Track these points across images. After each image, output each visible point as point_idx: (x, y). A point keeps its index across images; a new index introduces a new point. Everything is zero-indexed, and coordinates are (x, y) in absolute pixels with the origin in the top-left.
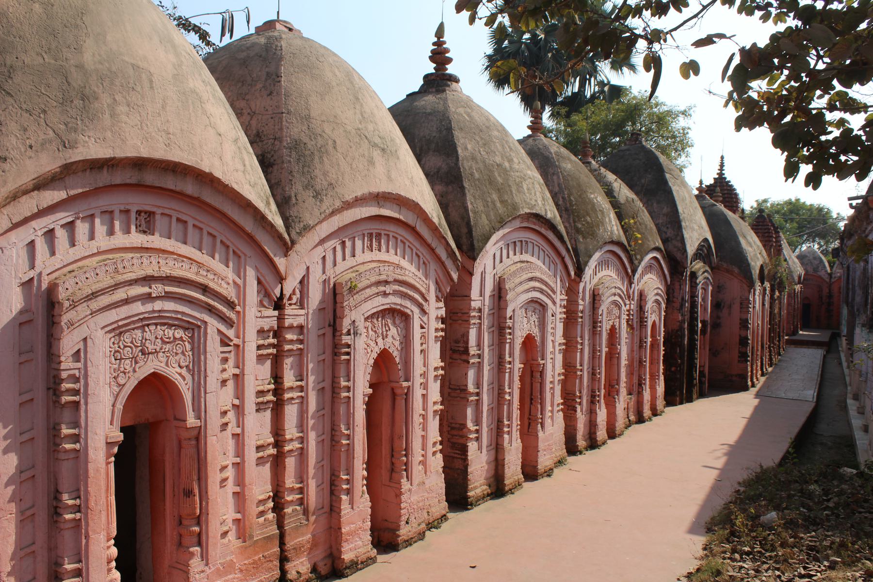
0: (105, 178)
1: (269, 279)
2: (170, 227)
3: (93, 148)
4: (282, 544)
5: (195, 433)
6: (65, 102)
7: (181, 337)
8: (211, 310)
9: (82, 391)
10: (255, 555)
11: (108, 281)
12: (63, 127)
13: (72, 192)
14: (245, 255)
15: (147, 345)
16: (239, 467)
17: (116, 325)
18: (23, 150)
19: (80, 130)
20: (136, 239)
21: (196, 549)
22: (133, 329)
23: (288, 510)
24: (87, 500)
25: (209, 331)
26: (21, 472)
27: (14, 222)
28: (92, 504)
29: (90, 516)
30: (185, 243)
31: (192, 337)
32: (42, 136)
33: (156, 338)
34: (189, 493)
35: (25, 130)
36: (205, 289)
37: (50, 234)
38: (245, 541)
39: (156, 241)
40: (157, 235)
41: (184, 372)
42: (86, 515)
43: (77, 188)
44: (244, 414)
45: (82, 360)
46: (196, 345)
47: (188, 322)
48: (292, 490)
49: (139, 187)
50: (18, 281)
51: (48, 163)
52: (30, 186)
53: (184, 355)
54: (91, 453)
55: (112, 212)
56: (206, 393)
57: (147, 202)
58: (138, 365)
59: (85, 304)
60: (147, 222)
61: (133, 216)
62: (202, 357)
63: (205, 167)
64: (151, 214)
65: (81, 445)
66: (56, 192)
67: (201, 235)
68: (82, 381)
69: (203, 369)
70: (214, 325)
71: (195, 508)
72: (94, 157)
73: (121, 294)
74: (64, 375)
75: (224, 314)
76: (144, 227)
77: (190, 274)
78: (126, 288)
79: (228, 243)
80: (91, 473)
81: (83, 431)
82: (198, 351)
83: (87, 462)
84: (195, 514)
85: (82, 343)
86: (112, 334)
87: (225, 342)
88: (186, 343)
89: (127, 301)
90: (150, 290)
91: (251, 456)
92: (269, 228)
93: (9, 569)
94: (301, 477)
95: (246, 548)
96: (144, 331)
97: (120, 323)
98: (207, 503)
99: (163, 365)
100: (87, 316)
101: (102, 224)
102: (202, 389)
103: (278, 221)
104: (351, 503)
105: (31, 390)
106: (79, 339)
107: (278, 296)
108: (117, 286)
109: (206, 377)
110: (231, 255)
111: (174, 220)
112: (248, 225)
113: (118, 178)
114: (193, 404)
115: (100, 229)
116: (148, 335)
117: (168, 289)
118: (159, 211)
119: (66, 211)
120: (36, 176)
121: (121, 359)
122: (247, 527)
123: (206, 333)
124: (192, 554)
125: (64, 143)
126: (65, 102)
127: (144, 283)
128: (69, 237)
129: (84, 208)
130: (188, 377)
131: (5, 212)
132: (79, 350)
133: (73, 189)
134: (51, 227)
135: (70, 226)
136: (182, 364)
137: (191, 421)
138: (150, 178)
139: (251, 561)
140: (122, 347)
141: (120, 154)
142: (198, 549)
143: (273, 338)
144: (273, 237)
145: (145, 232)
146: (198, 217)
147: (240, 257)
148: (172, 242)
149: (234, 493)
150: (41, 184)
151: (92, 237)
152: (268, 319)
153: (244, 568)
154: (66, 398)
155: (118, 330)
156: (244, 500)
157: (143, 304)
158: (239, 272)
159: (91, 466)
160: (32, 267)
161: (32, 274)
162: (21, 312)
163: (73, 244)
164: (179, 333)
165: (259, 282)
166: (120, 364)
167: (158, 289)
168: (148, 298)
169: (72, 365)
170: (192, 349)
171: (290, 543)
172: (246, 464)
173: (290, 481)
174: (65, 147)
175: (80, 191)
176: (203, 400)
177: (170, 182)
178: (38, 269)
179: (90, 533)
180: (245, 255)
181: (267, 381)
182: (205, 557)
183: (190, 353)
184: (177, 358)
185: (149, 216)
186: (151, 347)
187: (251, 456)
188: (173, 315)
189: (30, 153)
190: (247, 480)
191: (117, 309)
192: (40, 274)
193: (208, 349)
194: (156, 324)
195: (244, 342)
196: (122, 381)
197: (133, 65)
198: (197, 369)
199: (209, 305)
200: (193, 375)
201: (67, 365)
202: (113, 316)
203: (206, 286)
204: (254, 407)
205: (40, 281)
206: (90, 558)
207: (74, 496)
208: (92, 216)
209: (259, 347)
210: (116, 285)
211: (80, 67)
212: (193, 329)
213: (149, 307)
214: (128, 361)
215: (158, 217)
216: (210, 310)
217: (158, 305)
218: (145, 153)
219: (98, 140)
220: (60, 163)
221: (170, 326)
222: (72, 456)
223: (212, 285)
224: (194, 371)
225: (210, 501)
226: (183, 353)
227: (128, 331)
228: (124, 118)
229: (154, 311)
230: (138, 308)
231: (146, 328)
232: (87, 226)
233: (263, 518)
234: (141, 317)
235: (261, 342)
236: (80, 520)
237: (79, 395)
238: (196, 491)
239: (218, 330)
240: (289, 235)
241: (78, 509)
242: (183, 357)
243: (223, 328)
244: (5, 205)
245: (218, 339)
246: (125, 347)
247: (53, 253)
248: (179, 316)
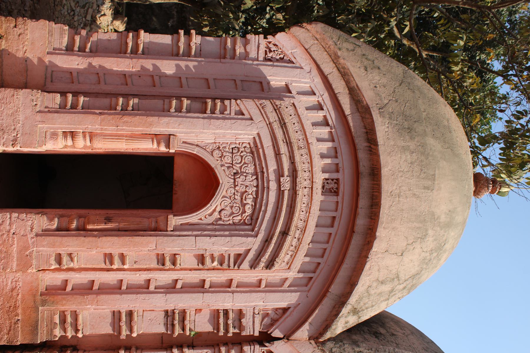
0: (361, 144)
1: (288, 321)
2: (328, 211)
3: (382, 129)
5: (162, 226)
7: (245, 212)
8: (267, 241)
9: (213, 115)
10: (23, 309)
12: (390, 110)
13: (350, 118)
14: (308, 291)
15: (242, 177)
17: (259, 146)
18: (373, 82)
19: (391, 121)
20: (320, 177)
21: (55, 224)
22: (255, 165)
24: (130, 115)
25: (250, 239)
26: (160, 77)
27: (328, 76)
28: (126, 119)
29: (117, 116)
30: (316, 226)
31: (245, 224)
32: (383, 96)
33: (247, 186)
35: (384, 87)
36: (285, 233)
37: (320, 107)
38: (41, 295)
39: (318, 197)
40: (322, 198)
41: (216, 215)
42: (118, 114)
43: (353, 122)
44: (166, 293)
45: (236, 116)
46: (238, 227)
47: (257, 219)
49: (357, 174)
50: (289, 82)
51: (369, 96)
52: (353, 84)
53: (230, 215)
54: (165, 120)
55: (336, 157)
56: (196, 236)
57: (346, 187)
58: (226, 169)
59: (277, 118)
60: (331, 189)
61: (335, 176)
62: (227, 233)
63: (381, 232)
64: (336, 193)
65: (173, 112)
66: (349, 106)
67: (323, 243)
68: (221, 116)
69: (217, 233)
70: (254, 244)
71: (94, 223)
72: (377, 129)
73: (283, 149)
74: (227, 102)
75: (263, 255)
76: (327, 186)
77: (297, 221)
78: (288, 154)
79: (318, 271)
80: (151, 119)
81: (183, 114)
82: (233, 229)
83: (159, 116)
84: (89, 223)
85: (249, 117)
86: (252, 145)
87: (239, 258)
88: (239, 218)
89: (278, 154)
90: (286, 176)
91: (124, 303)
92: (334, 313)
93: (94, 64)
95: (34, 296)
96: (253, 175)
97: (261, 150)
98: (95, 236)
99: (224, 193)
100: (268, 119)
101: (328, 148)
102: (199, 233)
103: (339, 327)
105: (216, 88)
106: (252, 114)
107: (273, 335)
109: (210, 236)
110: (309, 273)
111: (329, 230)
112: (335, 289)
113: (362, 155)
114: (187, 224)
116: (249, 177)
117: (286, 193)
119: (336, 119)
120: (360, 86)
121: (232, 153)
122: (56, 298)
123: (247, 236)
124: (51, 220)
125: (382, 109)
127: (291, 171)
128: (318, 122)
129: (339, 132)
130: (211, 220)
131: (334, 70)
132: (243, 114)
133: (352, 119)
134: (325, 108)
135: (326, 123)
136: (223, 212)
137: (174, 221)
138: (365, 183)
139: (19, 303)
140: (242, 154)
141: (382, 149)
142: (55, 226)
143: (233, 333)
144: (327, 320)
145: (323, 187)
146: (337, 237)
147: (307, 286)
148: (318, 213)
149: (93, 281)
150: (354, 93)
151: (319, 140)
152: (251, 323)
153: (15, 294)
156: (83, 294)
157: (274, 170)
158: (295, 285)
159: (155, 119)
160: (299, 93)
161: (294, 92)
163: (314, 124)
164: (249, 210)
165: (285, 310)
166: (228, 152)
168: (280, 174)
169: (234, 108)
170: (234, 224)
172: (118, 296)
174: (379, 109)
175: (351, 124)
176: (190, 233)
177: (363, 202)
178: (297, 96)
179: (102, 116)
180: (308, 291)
181: (192, 328)
182: (46, 233)
183: (231, 222)
184: (228, 208)
185: (335, 192)
187: (124, 303)
188: (264, 202)
189: (372, 86)
191: (272, 147)
192: (294, 98)
193: (234, 238)
194: (257, 186)
195: (233, 292)
196: (217, 153)
197: (434, 175)
198: (217, 228)
199: (271, 238)
200: (212, 224)
201: (233, 106)
202: (267, 143)
203: (287, 234)
204: (170, 307)
205: (289, 97)
206: (83, 115)
207: (134, 107)
208: (333, 141)
209: (226, 312)
210: (291, 143)
212: (251, 224)
213: (272, 177)
214: (230, 159)
215: (334, 199)
216: (267, 241)
217: (273, 185)
218: (385, 171)
219: (387, 133)
220: (369, 103)
221: (255, 200)
222: (166, 107)
223: (289, 238)
224: (216, 225)
225: (97, 239)
226: (233, 213)
227: (253, 158)
228: (404, 157)
229: (268, 181)
230: (272, 166)
231: (254, 177)
232: (326, 136)
233: (57, 321)
234: (265, 170)
235: (231, 315)
236: (116, 109)
237: (211, 113)
238: (109, 226)
239: (249, 250)
240: (329, 340)
242: (229, 213)
243: (251, 256)
244: (339, 70)
245: (241, 250)
246: (242, 157)
247: (307, 109)
248: (263, 208)
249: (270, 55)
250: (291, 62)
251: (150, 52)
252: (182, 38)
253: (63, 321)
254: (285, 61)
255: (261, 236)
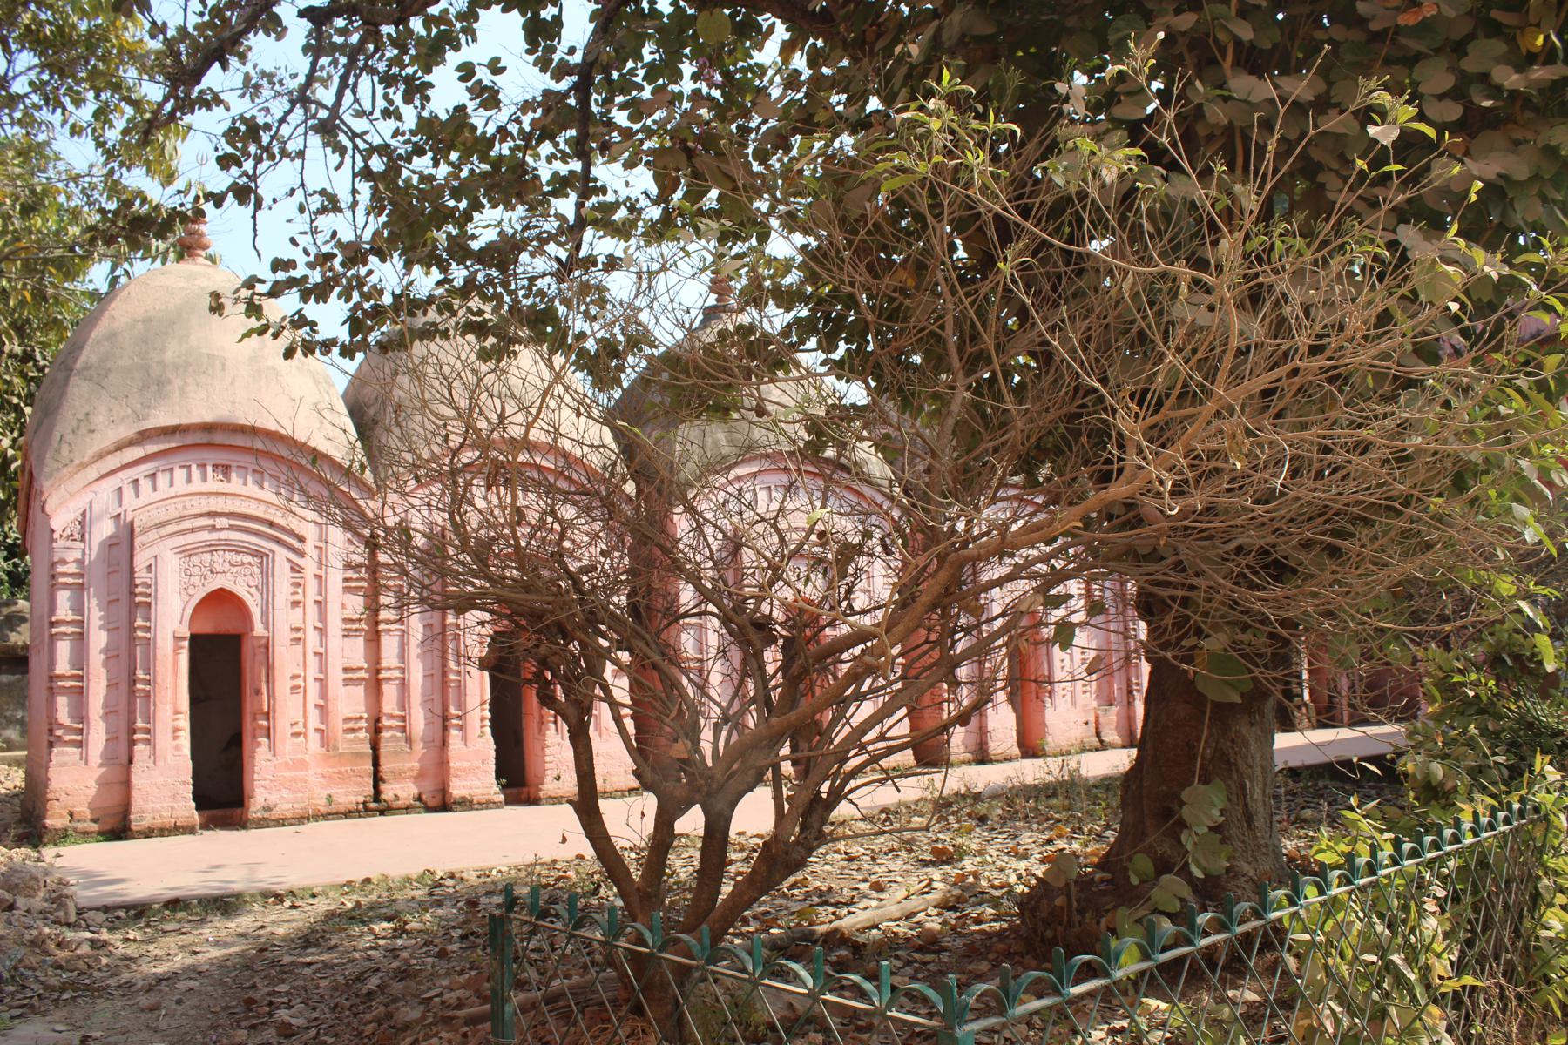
4: (376, 763)
6: (145, 387)
8: (279, 541)
11: (174, 514)
16: (323, 683)
20: (214, 484)
21: (264, 741)
23: (385, 734)
28: (159, 680)
34: (258, 692)
36: (271, 524)
41: (253, 590)
48: (392, 716)
51: (126, 431)
54: (159, 642)
70: (282, 553)
73: (187, 524)
82: (267, 574)
87: (295, 569)
89: (192, 530)
91: (336, 676)
94: (403, 703)
104: (465, 739)
108: (183, 518)
113: (190, 440)
115: (180, 474)
118: (234, 464)
124: (259, 744)
126: (145, 387)
135: (153, 476)
137: (259, 629)
138: (219, 438)
141: (185, 421)
150: (120, 447)
154: (138, 599)
155: (188, 552)
162: (110, 537)
164: (248, 559)
167: (222, 522)
168: (213, 528)
171: (386, 766)
173: (390, 703)
177: (240, 441)
182: (272, 748)
186: (218, 568)
187: (336, 676)
190: (330, 694)
196: (191, 591)
201: (141, 575)
211: (161, 362)
213: (215, 535)
217: (224, 535)
221: (238, 553)
223: (277, 520)
230: (205, 535)
241: (148, 683)
245: (288, 565)
249: (77, 536)
250: (84, 514)
251: (80, 658)
252: (62, 629)
253: (352, 730)
254: (84, 522)
255: (274, 547)
